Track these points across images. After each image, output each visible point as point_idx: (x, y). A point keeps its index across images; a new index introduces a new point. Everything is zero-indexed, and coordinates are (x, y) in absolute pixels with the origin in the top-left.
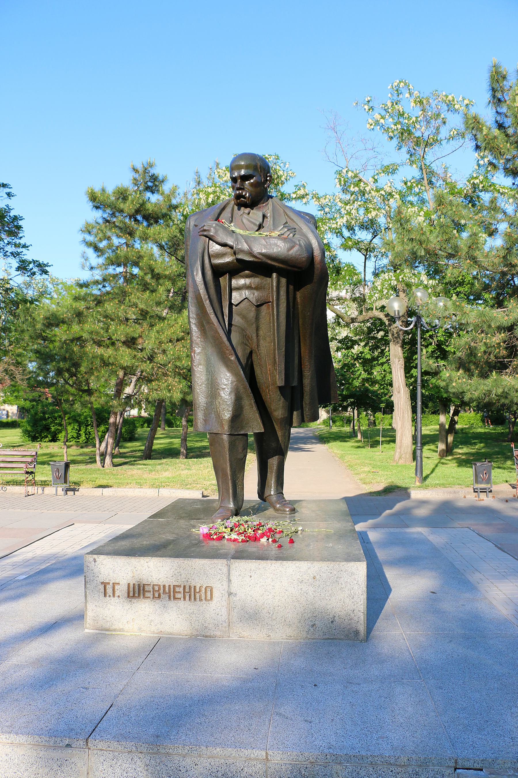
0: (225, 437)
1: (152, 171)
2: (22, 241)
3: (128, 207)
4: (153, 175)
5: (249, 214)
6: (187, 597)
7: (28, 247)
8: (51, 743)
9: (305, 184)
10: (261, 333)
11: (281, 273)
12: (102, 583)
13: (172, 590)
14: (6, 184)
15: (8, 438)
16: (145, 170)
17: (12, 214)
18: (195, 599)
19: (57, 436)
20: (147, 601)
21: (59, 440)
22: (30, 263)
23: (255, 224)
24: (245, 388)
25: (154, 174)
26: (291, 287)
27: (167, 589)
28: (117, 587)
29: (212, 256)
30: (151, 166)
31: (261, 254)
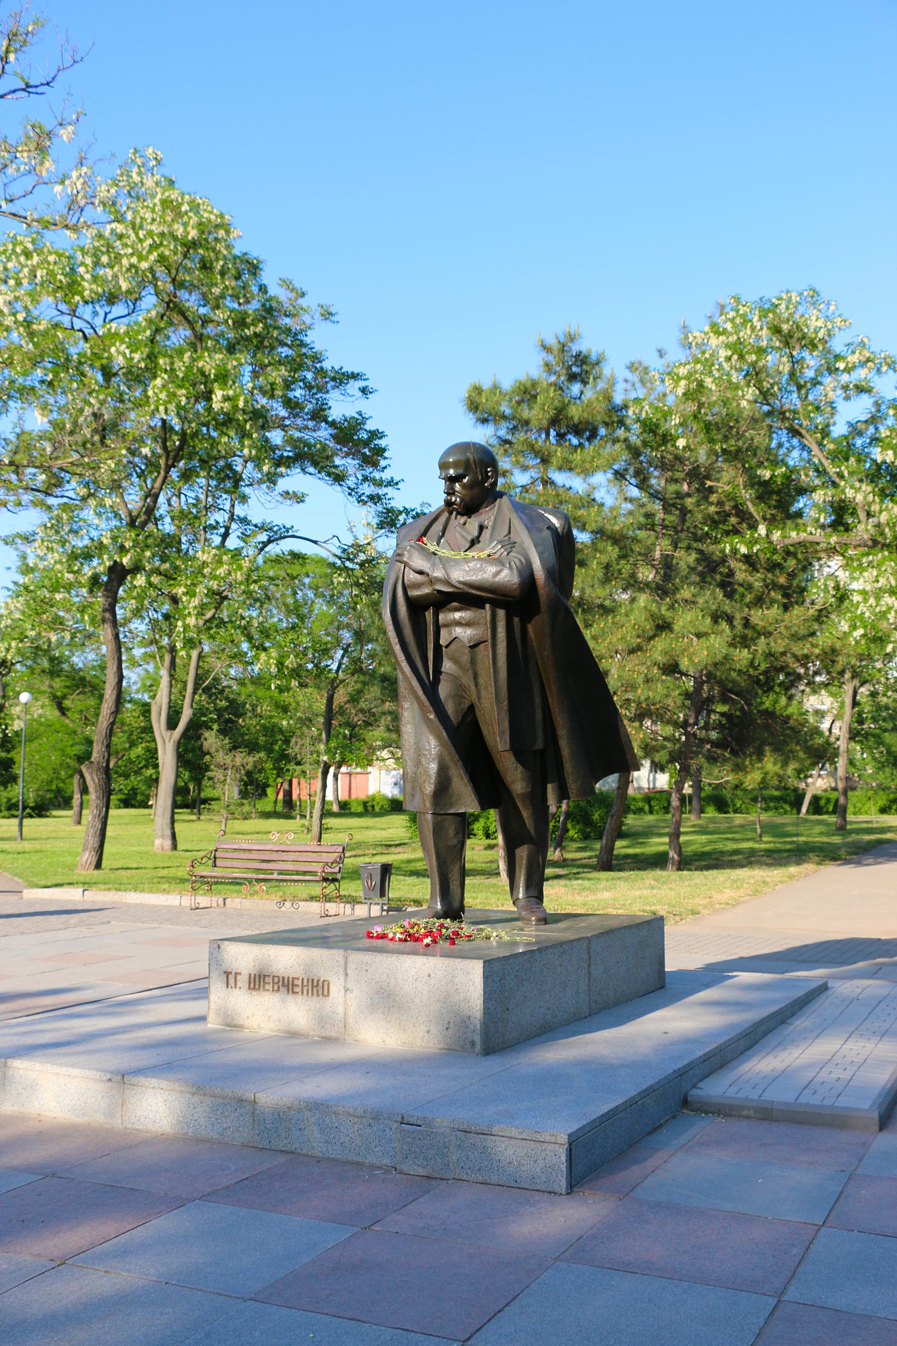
0: (429, 817)
1: (575, 348)
2: (386, 475)
3: (537, 414)
4: (578, 355)
5: (465, 524)
6: (305, 992)
7: (397, 484)
8: (98, 1077)
9: (865, 340)
10: (481, 681)
12: (225, 972)
14: (358, 374)
15: (391, 831)
16: (563, 348)
17: (370, 426)
18: (312, 994)
19: (471, 827)
20: (267, 993)
21: (475, 835)
22: (401, 513)
23: (467, 540)
24: (450, 754)
25: (581, 352)
26: (516, 620)
27: (286, 982)
28: (239, 977)
29: (409, 587)
30: (572, 338)
31: (461, 582)
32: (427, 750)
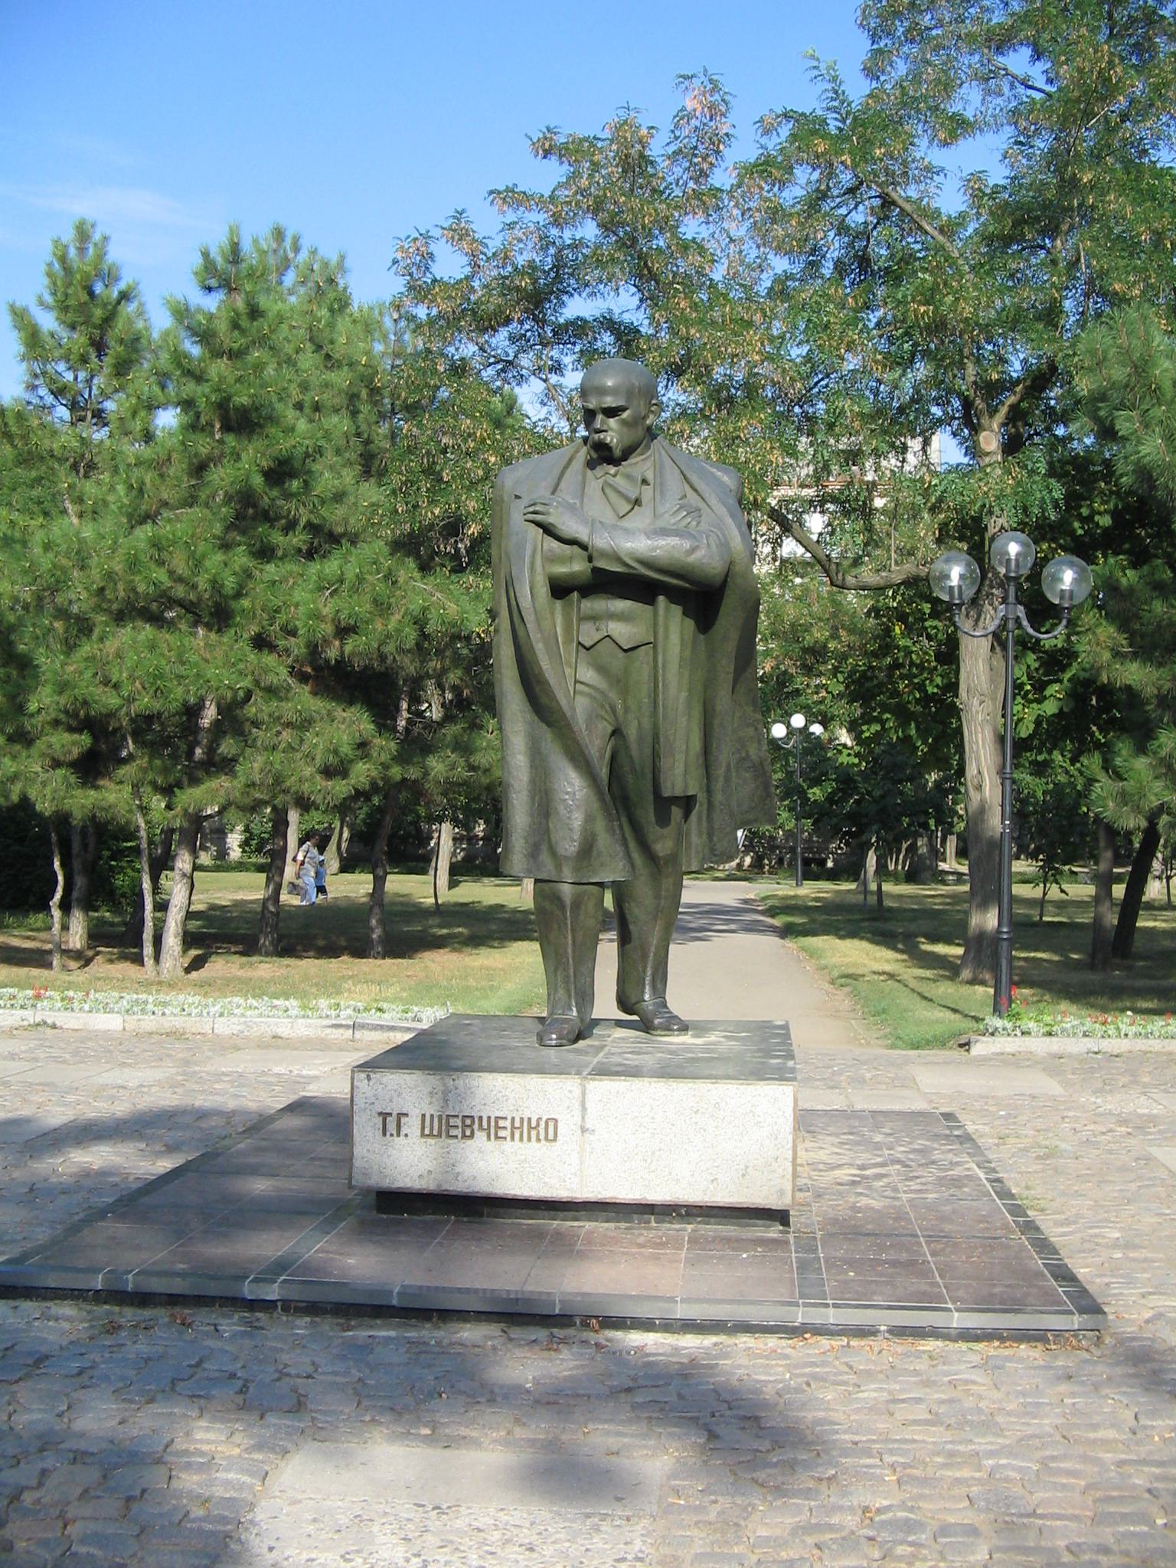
11: (675, 595)
12: (380, 1114)
13: (493, 1124)
18: (529, 1139)
28: (403, 1120)
32: (567, 793)
